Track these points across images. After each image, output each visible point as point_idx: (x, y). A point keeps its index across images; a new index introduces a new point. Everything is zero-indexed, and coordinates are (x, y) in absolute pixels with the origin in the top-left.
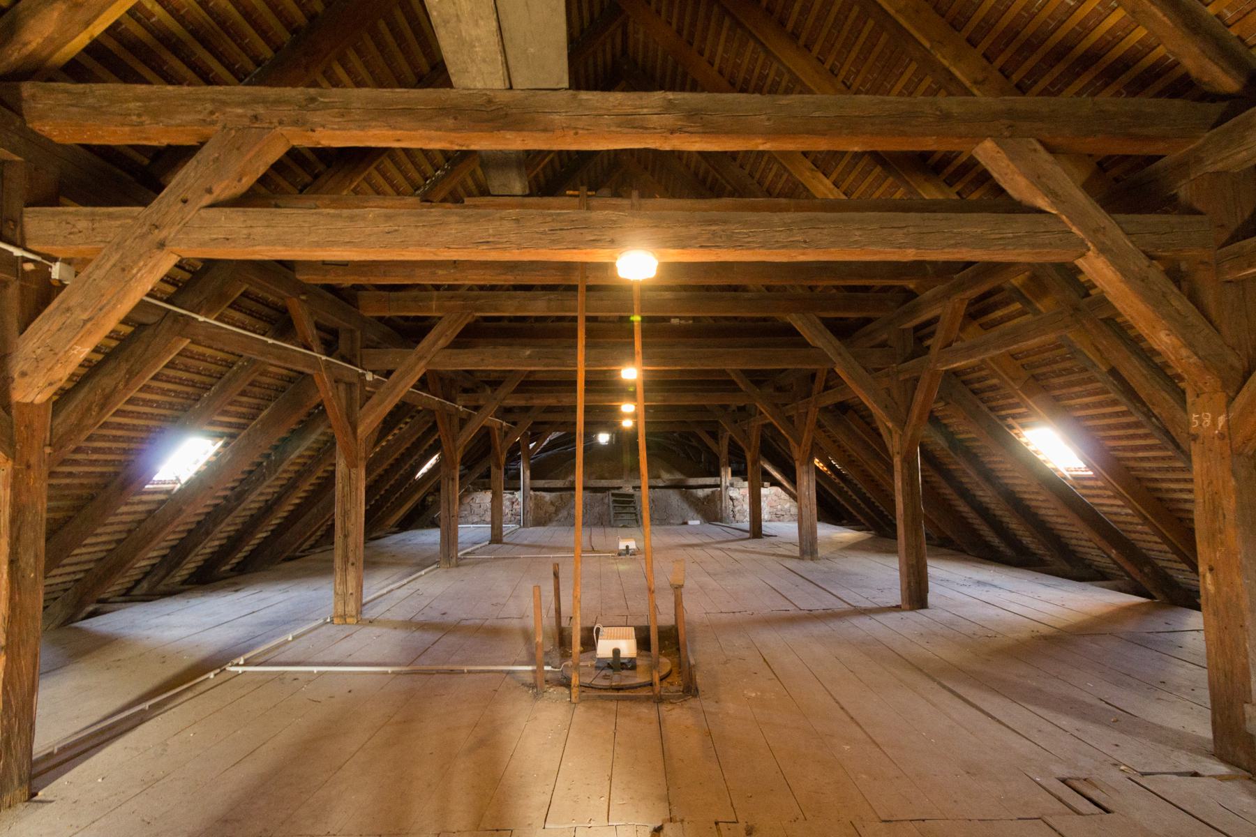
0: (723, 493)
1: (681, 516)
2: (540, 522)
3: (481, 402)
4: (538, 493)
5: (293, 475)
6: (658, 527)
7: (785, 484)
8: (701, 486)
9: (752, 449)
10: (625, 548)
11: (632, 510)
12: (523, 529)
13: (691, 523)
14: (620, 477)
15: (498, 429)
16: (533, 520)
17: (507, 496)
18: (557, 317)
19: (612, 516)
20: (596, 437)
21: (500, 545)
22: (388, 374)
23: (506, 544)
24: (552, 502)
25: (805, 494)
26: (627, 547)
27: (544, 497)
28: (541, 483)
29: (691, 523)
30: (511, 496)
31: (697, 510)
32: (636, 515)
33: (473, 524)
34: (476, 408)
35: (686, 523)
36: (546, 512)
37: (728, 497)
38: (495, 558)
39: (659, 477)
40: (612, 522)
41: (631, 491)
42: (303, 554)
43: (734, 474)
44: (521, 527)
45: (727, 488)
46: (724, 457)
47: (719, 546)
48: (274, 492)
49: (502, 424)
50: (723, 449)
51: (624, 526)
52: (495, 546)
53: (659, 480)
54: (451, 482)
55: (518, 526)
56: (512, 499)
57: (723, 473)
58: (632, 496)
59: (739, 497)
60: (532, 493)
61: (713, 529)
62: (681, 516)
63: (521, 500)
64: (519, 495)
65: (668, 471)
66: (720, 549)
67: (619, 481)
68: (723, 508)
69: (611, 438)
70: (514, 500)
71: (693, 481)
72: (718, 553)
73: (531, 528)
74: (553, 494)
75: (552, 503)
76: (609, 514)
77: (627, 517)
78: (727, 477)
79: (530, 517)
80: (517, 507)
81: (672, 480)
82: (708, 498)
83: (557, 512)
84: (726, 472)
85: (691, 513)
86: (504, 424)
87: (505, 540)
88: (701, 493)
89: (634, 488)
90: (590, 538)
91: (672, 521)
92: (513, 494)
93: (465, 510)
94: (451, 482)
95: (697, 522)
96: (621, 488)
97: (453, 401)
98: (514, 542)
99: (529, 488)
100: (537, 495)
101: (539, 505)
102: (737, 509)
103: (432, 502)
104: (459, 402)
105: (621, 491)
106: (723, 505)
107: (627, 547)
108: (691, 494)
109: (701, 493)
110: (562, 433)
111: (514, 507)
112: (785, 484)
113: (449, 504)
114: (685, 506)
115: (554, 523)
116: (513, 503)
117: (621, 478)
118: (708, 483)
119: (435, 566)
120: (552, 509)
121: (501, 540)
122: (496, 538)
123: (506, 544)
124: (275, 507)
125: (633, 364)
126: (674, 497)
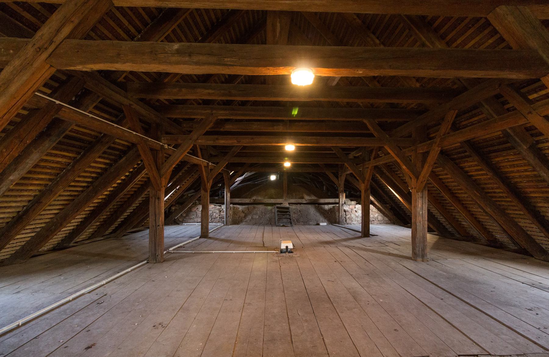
0: (340, 207)
1: (316, 220)
2: (236, 222)
3: (180, 141)
4: (235, 206)
5: (37, 193)
6: (303, 226)
7: (376, 203)
8: (328, 203)
9: (366, 182)
10: (285, 248)
11: (288, 216)
12: (225, 227)
13: (321, 224)
14: (281, 197)
15: (205, 167)
16: (232, 221)
17: (211, 207)
18: (242, 101)
19: (277, 220)
20: (269, 177)
21: (206, 239)
22: (217, 163)
23: (210, 238)
24: (243, 211)
25: (419, 213)
26: (287, 247)
27: (239, 208)
28: (237, 200)
29: (321, 224)
30: (219, 207)
31: (324, 216)
32: (290, 220)
33: (198, 223)
34: (176, 146)
35: (318, 224)
36: (239, 217)
37: (343, 210)
38: (195, 253)
39: (303, 198)
40: (277, 223)
41: (287, 206)
42: (75, 244)
43: (346, 197)
44: (224, 225)
45: (342, 205)
46: (342, 188)
47: (345, 243)
48: (24, 206)
49: (208, 164)
50: (341, 183)
51: (283, 226)
52: (203, 240)
53: (303, 200)
54: (157, 201)
55: (223, 224)
56: (220, 209)
57: (341, 196)
58: (288, 208)
59: (349, 210)
60: (231, 206)
61: (335, 228)
62: (316, 220)
63: (225, 210)
64: (224, 207)
65: (308, 195)
66: (348, 247)
67: (281, 200)
68: (340, 216)
69: (277, 177)
70: (221, 210)
71: (322, 201)
72: (348, 251)
73: (230, 226)
74: (244, 206)
75: (243, 212)
76: (275, 219)
77: (285, 220)
78: (343, 198)
79: (230, 220)
80: (223, 213)
81: (311, 200)
82: (332, 211)
83: (245, 217)
84: (342, 196)
85: (321, 218)
86: (210, 164)
87: (210, 235)
88: (327, 207)
89: (289, 204)
90: (263, 234)
91: (310, 223)
92: (221, 206)
93: (194, 215)
94: (157, 201)
95: (325, 224)
96: (282, 203)
97: (158, 139)
98: (216, 237)
99: (229, 203)
100: (234, 207)
101: (235, 212)
102: (347, 217)
103: (174, 210)
104: (163, 141)
105: (282, 206)
106: (340, 214)
107: (287, 247)
108: (322, 208)
109: (327, 207)
110: (253, 173)
111: (221, 213)
112: (376, 203)
113: (155, 217)
114: (318, 214)
115: (244, 223)
116: (220, 211)
117: (282, 198)
118: (331, 202)
119: (146, 262)
120: (243, 215)
121: (207, 236)
122: (205, 234)
123: (210, 238)
124: (24, 217)
125: (290, 75)
126: (312, 210)
